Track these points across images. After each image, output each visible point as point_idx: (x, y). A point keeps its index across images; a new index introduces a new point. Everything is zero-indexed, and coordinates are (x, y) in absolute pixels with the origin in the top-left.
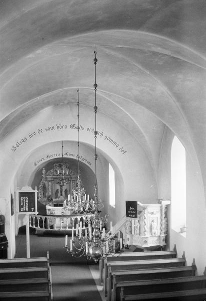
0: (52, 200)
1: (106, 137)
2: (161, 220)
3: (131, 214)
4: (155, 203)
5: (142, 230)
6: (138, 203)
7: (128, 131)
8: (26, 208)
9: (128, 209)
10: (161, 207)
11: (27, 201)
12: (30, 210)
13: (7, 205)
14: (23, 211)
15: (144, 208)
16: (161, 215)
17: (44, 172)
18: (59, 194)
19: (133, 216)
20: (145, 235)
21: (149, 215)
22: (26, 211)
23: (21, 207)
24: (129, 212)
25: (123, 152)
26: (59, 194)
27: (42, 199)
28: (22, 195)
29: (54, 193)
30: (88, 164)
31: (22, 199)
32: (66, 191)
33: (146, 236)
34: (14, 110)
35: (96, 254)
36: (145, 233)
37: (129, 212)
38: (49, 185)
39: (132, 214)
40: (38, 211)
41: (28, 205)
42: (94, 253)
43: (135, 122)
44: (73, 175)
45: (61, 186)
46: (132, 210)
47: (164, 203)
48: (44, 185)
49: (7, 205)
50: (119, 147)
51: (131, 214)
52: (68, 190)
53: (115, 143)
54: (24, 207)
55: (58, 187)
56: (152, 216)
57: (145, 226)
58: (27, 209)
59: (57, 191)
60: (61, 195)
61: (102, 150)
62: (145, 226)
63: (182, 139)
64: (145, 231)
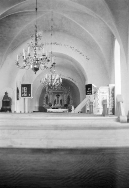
0: (52, 106)
1: (76, 50)
2: (110, 98)
3: (88, 93)
4: (106, 86)
5: (96, 104)
6: (93, 85)
7: (89, 45)
8: (25, 94)
9: (87, 90)
10: (109, 89)
11: (26, 90)
12: (28, 96)
13: (14, 92)
14: (24, 96)
15: (97, 89)
16: (109, 94)
17: (47, 89)
18: (57, 102)
19: (90, 93)
20: (98, 106)
21: (101, 94)
22: (25, 96)
23: (22, 93)
24: (87, 92)
25: (72, 48)
26: (57, 102)
27: (45, 105)
28: (23, 86)
29: (53, 101)
30: (73, 82)
31: (23, 89)
32: (61, 101)
33: (99, 107)
34: (4, 11)
35: (34, 67)
36: (98, 105)
37: (87, 92)
38: (50, 97)
39: (89, 92)
40: (33, 96)
41: (27, 93)
42: (34, 67)
43: (93, 37)
44: (66, 90)
45: (58, 98)
46: (89, 90)
47: (111, 86)
48: (47, 96)
49: (14, 92)
50: (85, 56)
51: (88, 93)
52: (62, 100)
53: (82, 54)
54: (24, 94)
55: (56, 98)
56: (103, 94)
57: (98, 101)
58: (26, 95)
59: (55, 100)
60: (58, 103)
61: (79, 62)
62: (98, 101)
63: (118, 40)
64: (98, 104)
